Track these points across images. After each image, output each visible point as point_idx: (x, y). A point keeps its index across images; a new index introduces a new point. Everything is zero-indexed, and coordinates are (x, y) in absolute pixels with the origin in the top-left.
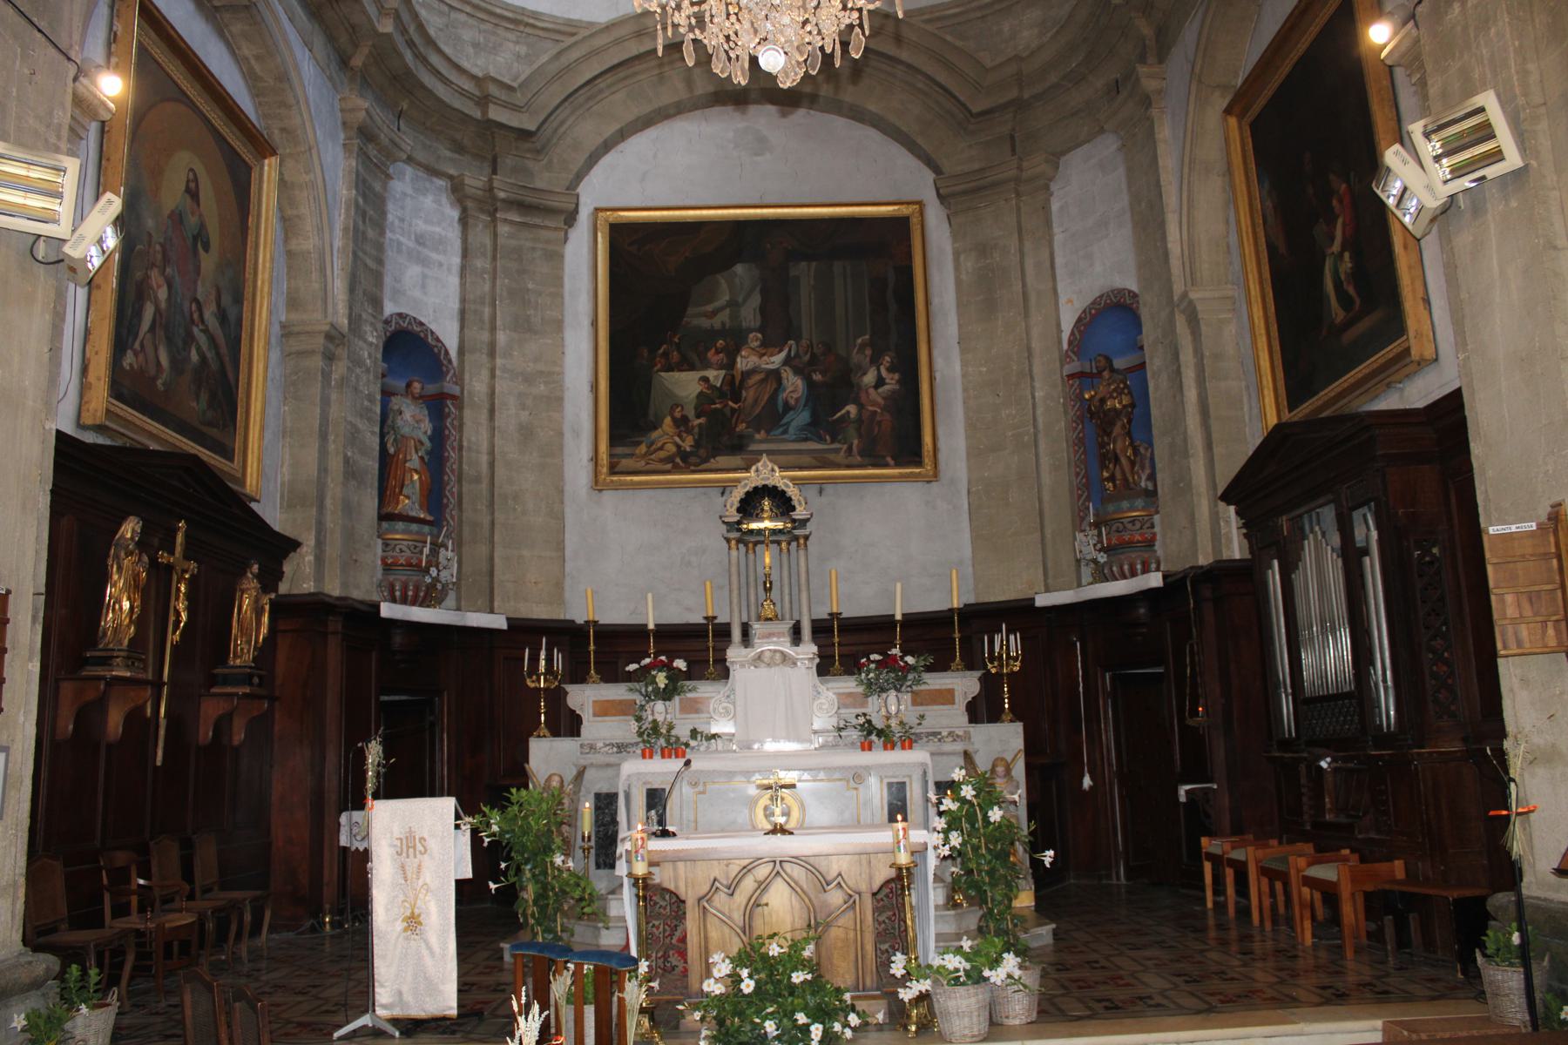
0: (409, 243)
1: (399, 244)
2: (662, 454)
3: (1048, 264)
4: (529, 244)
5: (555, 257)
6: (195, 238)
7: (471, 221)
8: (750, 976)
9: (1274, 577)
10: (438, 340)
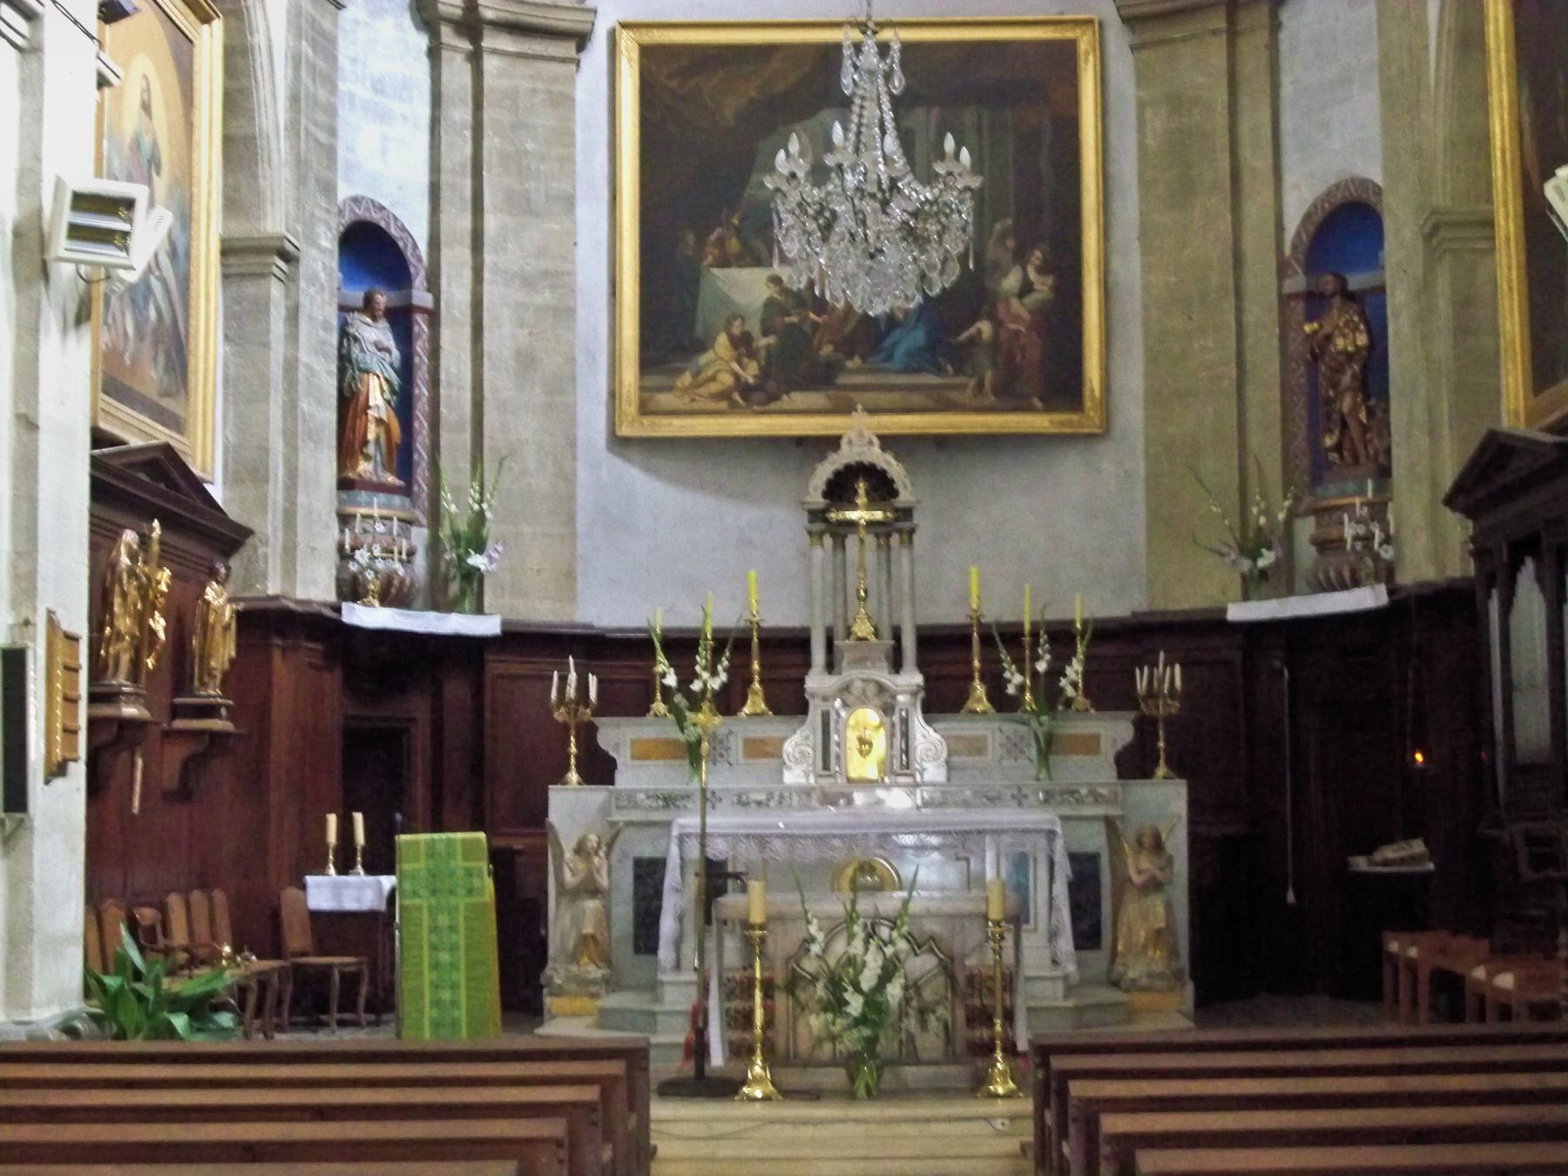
0: (364, 93)
1: (352, 96)
2: (714, 387)
3: (1267, 131)
4: (528, 85)
6: (149, 162)
7: (445, 54)
9: (1494, 607)
10: (403, 229)
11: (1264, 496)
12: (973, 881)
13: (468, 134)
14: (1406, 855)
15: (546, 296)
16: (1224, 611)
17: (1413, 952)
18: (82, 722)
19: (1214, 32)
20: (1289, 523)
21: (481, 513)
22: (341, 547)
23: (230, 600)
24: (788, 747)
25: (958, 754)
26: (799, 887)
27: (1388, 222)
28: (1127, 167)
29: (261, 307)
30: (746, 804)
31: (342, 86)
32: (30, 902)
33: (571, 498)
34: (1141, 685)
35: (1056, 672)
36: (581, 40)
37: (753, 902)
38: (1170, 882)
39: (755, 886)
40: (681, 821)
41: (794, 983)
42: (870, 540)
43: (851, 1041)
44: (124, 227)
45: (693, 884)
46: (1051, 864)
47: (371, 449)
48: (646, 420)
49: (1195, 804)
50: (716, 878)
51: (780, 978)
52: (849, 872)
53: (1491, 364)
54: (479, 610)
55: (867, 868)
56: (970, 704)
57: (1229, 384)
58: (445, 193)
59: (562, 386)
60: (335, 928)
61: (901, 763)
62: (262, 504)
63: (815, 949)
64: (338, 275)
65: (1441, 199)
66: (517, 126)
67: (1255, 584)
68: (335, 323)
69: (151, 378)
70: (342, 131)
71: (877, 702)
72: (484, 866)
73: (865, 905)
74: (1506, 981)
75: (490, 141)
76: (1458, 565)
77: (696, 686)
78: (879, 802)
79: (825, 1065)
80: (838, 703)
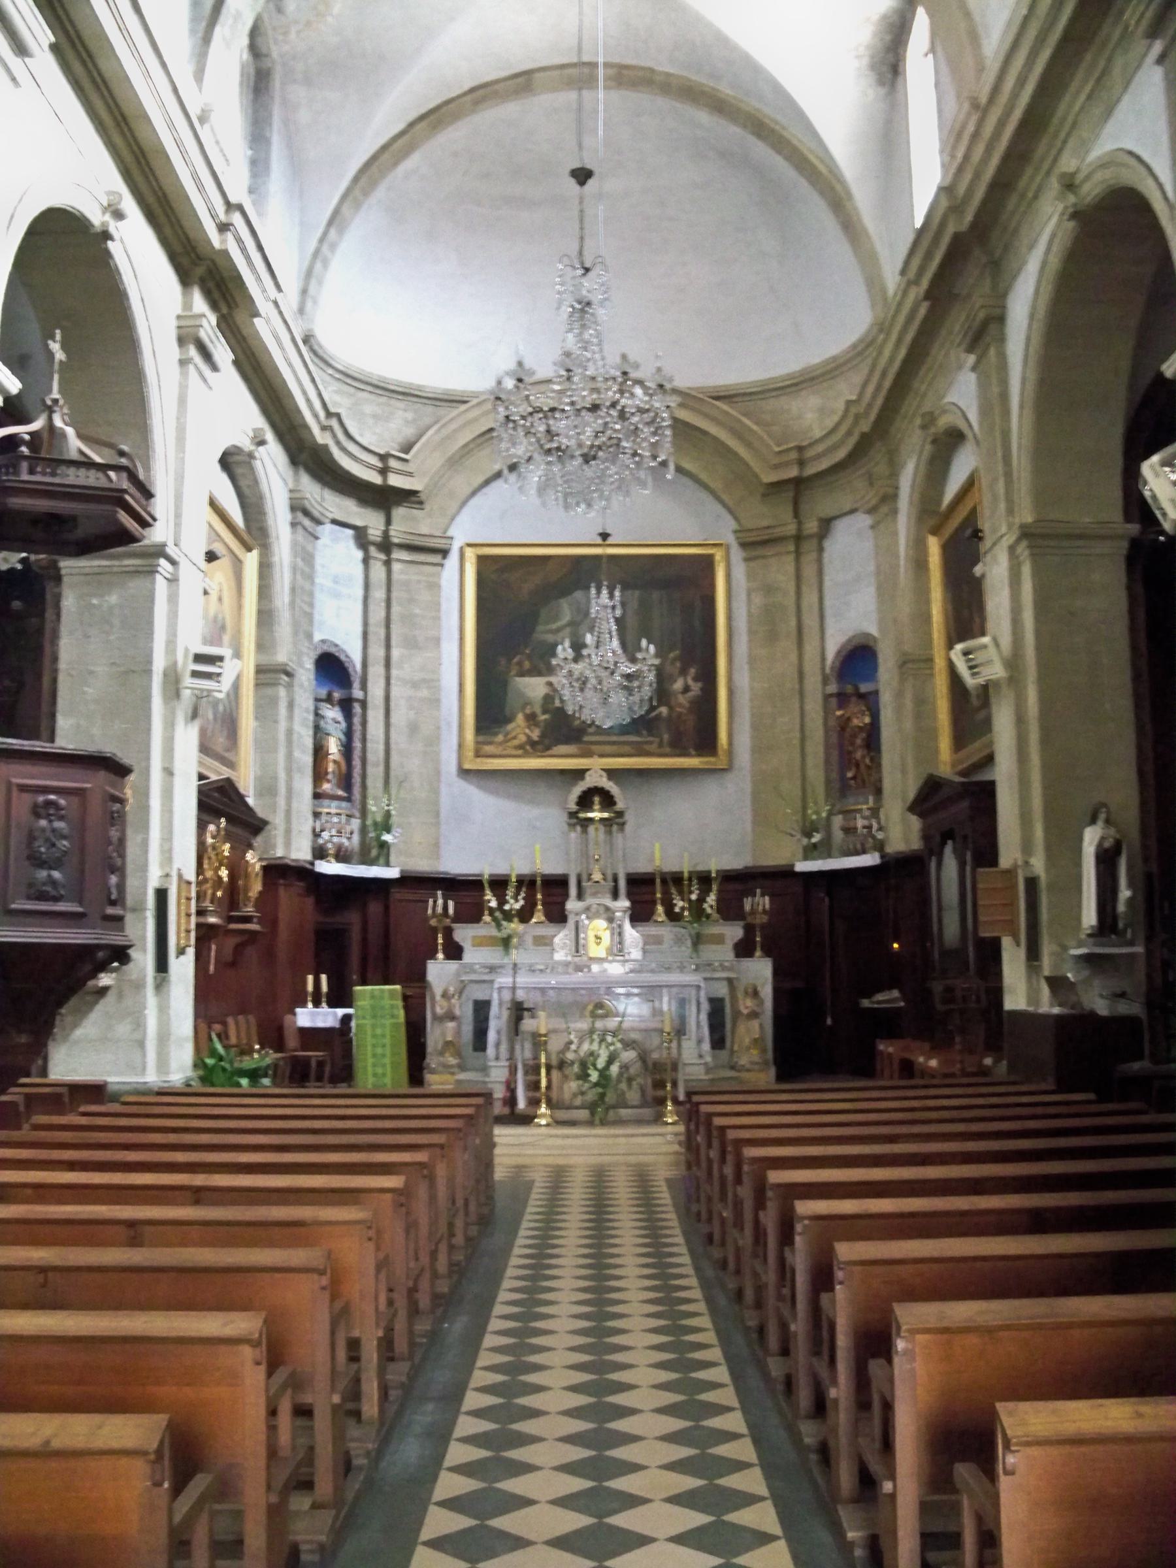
0: (328, 583)
2: (516, 742)
5: (434, 587)
7: (372, 562)
8: (615, 392)
10: (347, 656)
11: (816, 803)
12: (657, 1013)
13: (383, 604)
14: (888, 998)
15: (424, 693)
16: (793, 866)
17: (891, 1050)
18: (193, 926)
19: (788, 553)
20: (828, 818)
21: (388, 812)
22: (314, 830)
23: (260, 859)
24: (556, 940)
25: (649, 942)
26: (564, 1015)
27: (881, 660)
28: (741, 624)
29: (274, 701)
30: (534, 971)
31: (317, 581)
32: (169, 1019)
33: (436, 803)
34: (747, 907)
35: (701, 900)
36: (444, 553)
37: (540, 1023)
38: (763, 1012)
39: (542, 1014)
40: (499, 980)
41: (562, 1065)
42: (602, 828)
43: (591, 1096)
44: (217, 670)
45: (505, 1014)
46: (698, 1004)
47: (330, 777)
48: (479, 760)
49: (776, 973)
50: (519, 1011)
51: (554, 1062)
52: (590, 1007)
53: (933, 734)
54: (387, 864)
55: (600, 1005)
56: (655, 918)
57: (796, 742)
58: (371, 637)
59: (433, 741)
60: (310, 1036)
61: (618, 949)
62: (274, 808)
63: (573, 1047)
64: (314, 682)
65: (907, 647)
66: (411, 600)
67: (811, 852)
68: (312, 708)
69: (220, 742)
70: (317, 604)
71: (605, 916)
72: (400, 1003)
73: (599, 1024)
74: (933, 1063)
75: (395, 609)
76: (916, 844)
77: (507, 907)
78: (605, 970)
79: (577, 1108)
80: (583, 917)
